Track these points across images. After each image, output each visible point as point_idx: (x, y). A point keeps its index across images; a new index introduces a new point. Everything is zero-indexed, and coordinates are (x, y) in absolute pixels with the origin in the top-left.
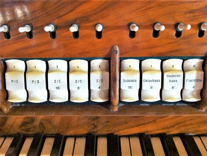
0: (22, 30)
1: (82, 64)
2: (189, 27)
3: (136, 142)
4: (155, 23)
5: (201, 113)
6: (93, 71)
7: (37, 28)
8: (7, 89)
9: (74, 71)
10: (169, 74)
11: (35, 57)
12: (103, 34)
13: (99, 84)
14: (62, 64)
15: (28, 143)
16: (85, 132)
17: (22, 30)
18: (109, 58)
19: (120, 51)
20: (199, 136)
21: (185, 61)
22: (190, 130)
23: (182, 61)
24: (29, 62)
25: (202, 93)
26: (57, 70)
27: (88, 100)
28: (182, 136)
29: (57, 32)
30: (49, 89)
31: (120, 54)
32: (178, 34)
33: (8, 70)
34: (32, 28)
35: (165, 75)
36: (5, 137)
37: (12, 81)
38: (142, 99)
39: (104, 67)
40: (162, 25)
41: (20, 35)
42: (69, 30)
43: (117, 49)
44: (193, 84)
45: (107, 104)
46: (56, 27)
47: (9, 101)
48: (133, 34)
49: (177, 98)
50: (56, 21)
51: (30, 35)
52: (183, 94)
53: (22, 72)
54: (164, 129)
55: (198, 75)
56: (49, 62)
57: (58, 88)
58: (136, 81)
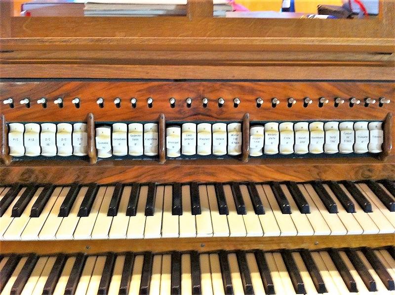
0: (22, 102)
1: (67, 127)
2: (389, 102)
3: (211, 189)
4: (273, 99)
5: (160, 164)
6: (114, 132)
7: (125, 100)
8: (9, 145)
9: (283, 131)
10: (132, 134)
11: (31, 121)
12: (80, 105)
13: (79, 142)
14: (320, 125)
15: (84, 191)
16: (70, 182)
17: (22, 102)
18: (242, 123)
19: (94, 117)
20: (303, 183)
21: (341, 124)
22: (155, 180)
23: (226, 125)
24: (27, 125)
25: (383, 147)
26: (361, 129)
27: (210, 153)
28: (287, 183)
29: (47, 103)
30: (73, 145)
31: (95, 119)
32: (336, 105)
33: (11, 131)
34: (29, 100)
35: (342, 132)
36: (5, 186)
37: (14, 139)
38: (325, 151)
39: (83, 129)
40: (342, 99)
41: (21, 106)
42: (53, 103)
43: (92, 116)
44: (151, 141)
45: (157, 158)
46: (46, 100)
47: (10, 154)
48: (236, 105)
49: (335, 151)
50: (47, 97)
51: (28, 105)
52: (310, 147)
53: (21, 132)
54: (135, 178)
55: (379, 132)
56: (42, 125)
57: (48, 145)
58: (367, 137)
